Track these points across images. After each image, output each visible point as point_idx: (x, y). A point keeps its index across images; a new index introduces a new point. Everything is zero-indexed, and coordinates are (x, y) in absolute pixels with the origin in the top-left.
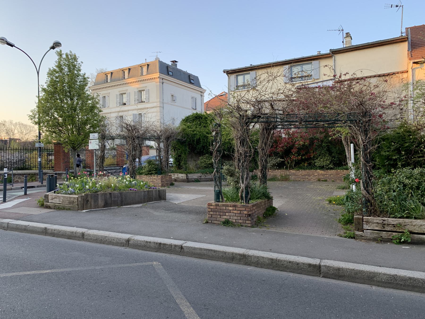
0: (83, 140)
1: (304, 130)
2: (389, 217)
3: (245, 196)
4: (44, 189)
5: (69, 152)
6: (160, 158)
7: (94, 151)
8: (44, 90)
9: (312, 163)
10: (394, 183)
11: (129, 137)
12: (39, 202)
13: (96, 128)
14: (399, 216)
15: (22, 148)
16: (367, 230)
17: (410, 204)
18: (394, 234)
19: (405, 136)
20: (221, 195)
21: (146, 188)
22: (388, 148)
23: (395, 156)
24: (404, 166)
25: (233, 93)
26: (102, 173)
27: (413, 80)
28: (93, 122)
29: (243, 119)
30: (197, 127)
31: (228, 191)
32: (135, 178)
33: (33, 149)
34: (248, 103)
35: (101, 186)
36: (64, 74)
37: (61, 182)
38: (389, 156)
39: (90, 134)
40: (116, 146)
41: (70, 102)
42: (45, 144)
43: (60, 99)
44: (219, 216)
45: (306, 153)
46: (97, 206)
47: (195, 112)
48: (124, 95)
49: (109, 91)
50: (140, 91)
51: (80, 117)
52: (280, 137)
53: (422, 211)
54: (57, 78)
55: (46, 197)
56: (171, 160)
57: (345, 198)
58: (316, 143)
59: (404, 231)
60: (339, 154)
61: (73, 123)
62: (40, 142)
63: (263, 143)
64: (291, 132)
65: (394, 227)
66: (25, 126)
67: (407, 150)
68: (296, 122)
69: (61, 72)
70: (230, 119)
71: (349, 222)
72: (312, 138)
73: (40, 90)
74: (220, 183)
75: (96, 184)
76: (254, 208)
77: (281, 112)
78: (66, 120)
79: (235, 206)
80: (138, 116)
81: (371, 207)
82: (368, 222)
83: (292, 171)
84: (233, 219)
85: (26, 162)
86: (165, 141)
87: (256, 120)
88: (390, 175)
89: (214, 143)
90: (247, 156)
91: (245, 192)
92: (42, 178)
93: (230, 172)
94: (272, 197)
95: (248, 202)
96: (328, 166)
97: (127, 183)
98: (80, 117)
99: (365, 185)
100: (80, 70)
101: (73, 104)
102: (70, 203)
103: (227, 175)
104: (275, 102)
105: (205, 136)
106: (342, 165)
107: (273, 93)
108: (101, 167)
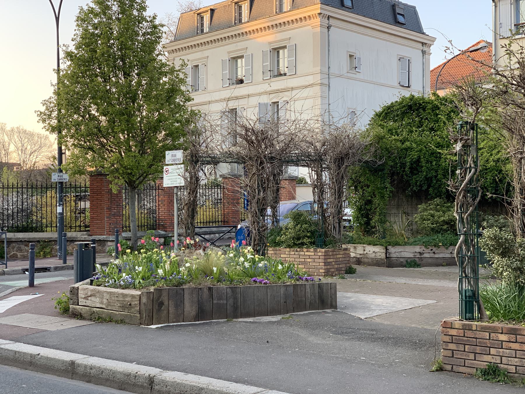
0: (150, 166)
4: (69, 275)
5: (120, 192)
6: (322, 207)
7: (175, 190)
8: (69, 55)
11: (250, 158)
12: (59, 303)
13: (178, 138)
15: (25, 184)
20: (478, 302)
21: (291, 277)
25: (507, 42)
26: (192, 242)
28: (172, 124)
31: (494, 294)
32: (263, 254)
33: (46, 187)
35: (189, 270)
36: (111, 19)
37: (104, 260)
39: (167, 152)
40: (220, 179)
41: (122, 80)
42: (70, 176)
43: (103, 75)
44: (472, 356)
46: (180, 317)
48: (239, 61)
49: (206, 53)
50: (276, 50)
51: (144, 112)
54: (96, 28)
55: (74, 292)
56: (349, 212)
61: (130, 127)
62: (61, 171)
66: (31, 135)
69: (105, 14)
70: (499, 109)
73: (62, 55)
74: (475, 271)
75: (179, 265)
78: (114, 123)
79: (513, 332)
80: (269, 108)
84: (510, 365)
85: (31, 213)
86: (332, 166)
92: (66, 250)
93: (500, 245)
97: (247, 265)
98: (144, 114)
100: (144, 9)
101: (130, 86)
102: (123, 307)
103: (492, 251)
105: (432, 154)
108: (190, 227)
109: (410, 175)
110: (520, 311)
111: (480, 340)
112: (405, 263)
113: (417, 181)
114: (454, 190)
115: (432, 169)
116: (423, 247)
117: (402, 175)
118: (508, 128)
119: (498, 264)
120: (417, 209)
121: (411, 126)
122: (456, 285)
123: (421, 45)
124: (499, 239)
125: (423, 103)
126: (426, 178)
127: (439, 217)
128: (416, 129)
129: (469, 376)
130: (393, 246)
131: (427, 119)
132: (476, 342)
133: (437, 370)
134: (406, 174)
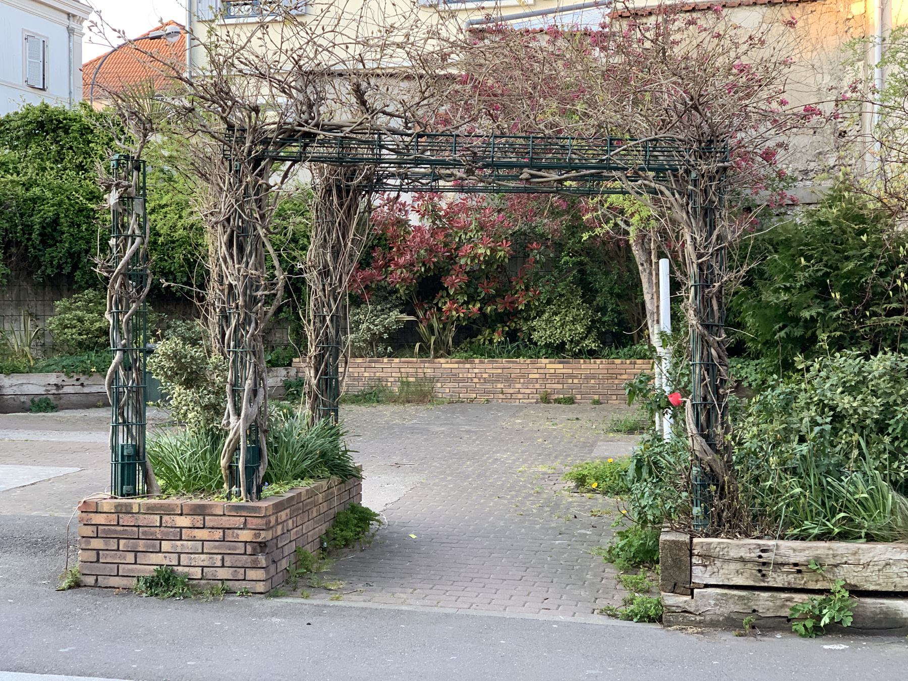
1: (494, 200)
2: (782, 538)
3: (246, 468)
9: (520, 330)
10: (802, 411)
14: (816, 531)
16: (707, 586)
17: (855, 486)
18: (798, 597)
19: (844, 232)
20: (143, 465)
22: (786, 279)
23: (809, 307)
24: (838, 345)
27: (883, 25)
29: (241, 141)
30: (44, 169)
34: (262, 76)
38: (788, 307)
44: (130, 558)
45: (500, 294)
47: (37, 104)
52: (402, 223)
53: (892, 513)
57: (632, 467)
58: (537, 253)
59: (832, 587)
60: (619, 296)
63: (324, 246)
64: (445, 207)
65: (799, 572)
67: (852, 285)
68: (456, 164)
71: (644, 557)
72: (524, 234)
74: (140, 413)
76: (283, 515)
77: (397, 123)
79: (200, 511)
81: (721, 499)
82: (708, 558)
83: (446, 364)
84: (192, 566)
87: (295, 149)
88: (790, 377)
89: (112, 242)
90: (255, 300)
91: (248, 449)
93: (182, 367)
94: (359, 469)
95: (259, 490)
96: (578, 343)
99: (703, 418)
103: (170, 378)
104: (373, 81)
105: (80, 211)
106: (631, 341)
107: (366, 43)
109: (41, 247)
110: (212, 476)
111: (146, 529)
112: (29, 403)
113: (53, 257)
114: (105, 274)
115: (81, 238)
116: (63, 375)
117: (26, 246)
118: (200, 172)
119: (179, 399)
120: (52, 309)
121: (42, 160)
122: (105, 438)
123: (66, 16)
124: (181, 358)
125: (65, 119)
126: (69, 253)
127: (92, 323)
128: (52, 165)
129: (125, 591)
130: (8, 374)
131: (71, 148)
132: (139, 533)
133: (70, 587)
134: (32, 245)
